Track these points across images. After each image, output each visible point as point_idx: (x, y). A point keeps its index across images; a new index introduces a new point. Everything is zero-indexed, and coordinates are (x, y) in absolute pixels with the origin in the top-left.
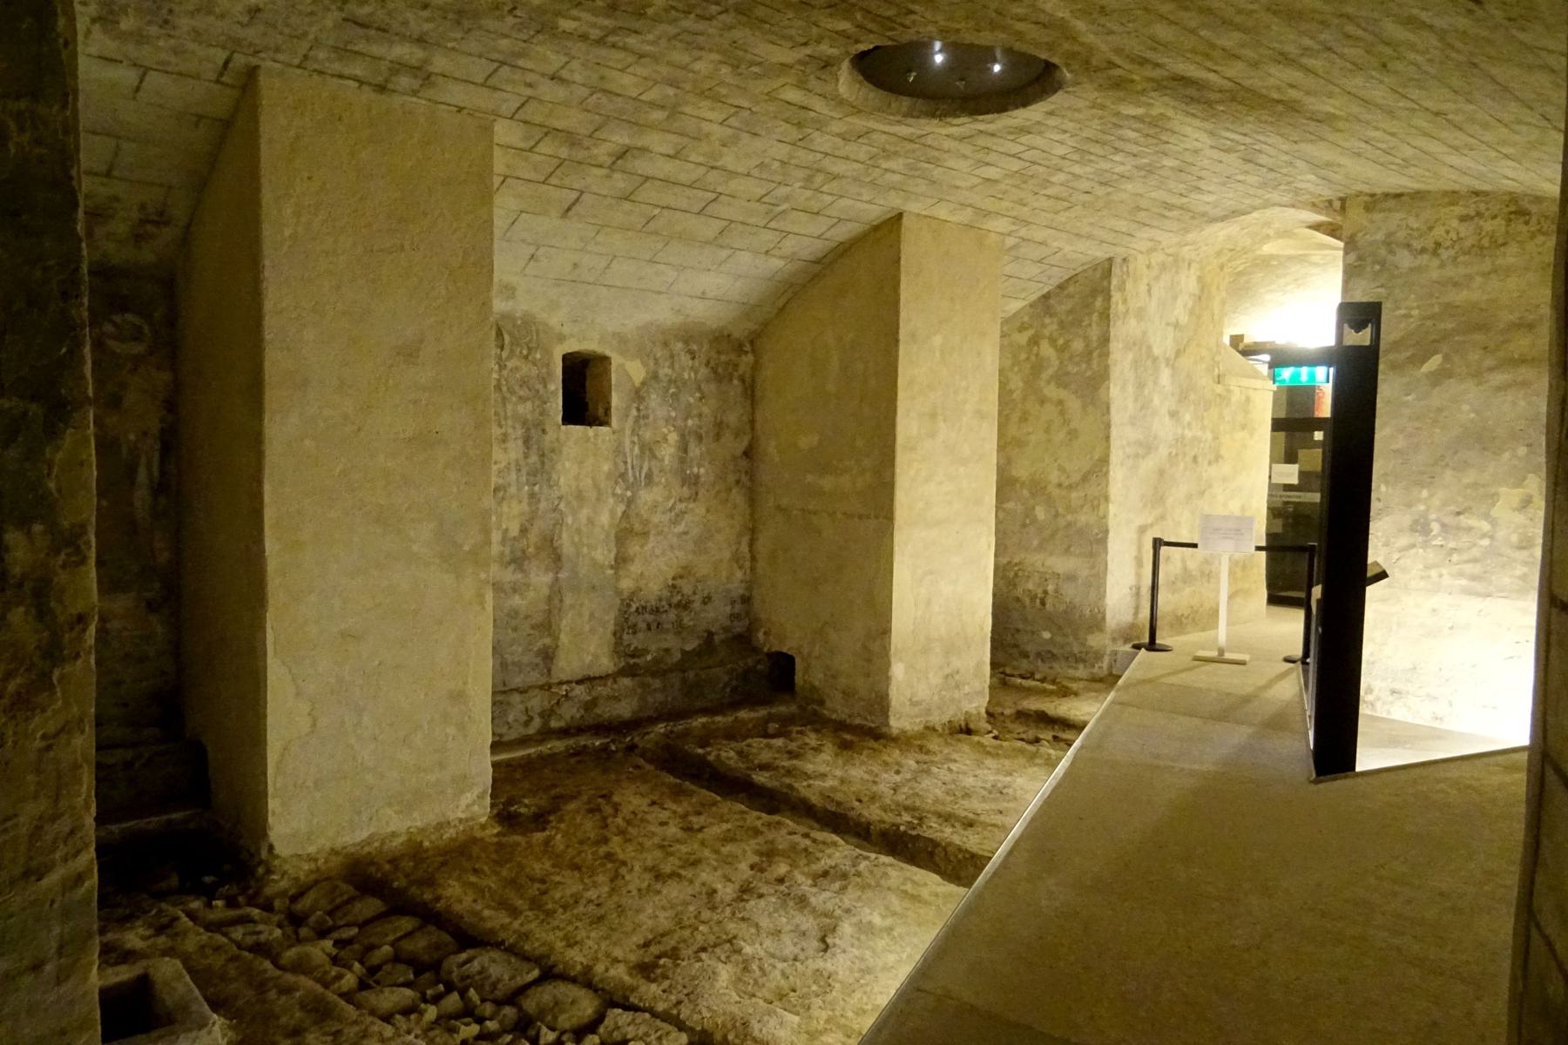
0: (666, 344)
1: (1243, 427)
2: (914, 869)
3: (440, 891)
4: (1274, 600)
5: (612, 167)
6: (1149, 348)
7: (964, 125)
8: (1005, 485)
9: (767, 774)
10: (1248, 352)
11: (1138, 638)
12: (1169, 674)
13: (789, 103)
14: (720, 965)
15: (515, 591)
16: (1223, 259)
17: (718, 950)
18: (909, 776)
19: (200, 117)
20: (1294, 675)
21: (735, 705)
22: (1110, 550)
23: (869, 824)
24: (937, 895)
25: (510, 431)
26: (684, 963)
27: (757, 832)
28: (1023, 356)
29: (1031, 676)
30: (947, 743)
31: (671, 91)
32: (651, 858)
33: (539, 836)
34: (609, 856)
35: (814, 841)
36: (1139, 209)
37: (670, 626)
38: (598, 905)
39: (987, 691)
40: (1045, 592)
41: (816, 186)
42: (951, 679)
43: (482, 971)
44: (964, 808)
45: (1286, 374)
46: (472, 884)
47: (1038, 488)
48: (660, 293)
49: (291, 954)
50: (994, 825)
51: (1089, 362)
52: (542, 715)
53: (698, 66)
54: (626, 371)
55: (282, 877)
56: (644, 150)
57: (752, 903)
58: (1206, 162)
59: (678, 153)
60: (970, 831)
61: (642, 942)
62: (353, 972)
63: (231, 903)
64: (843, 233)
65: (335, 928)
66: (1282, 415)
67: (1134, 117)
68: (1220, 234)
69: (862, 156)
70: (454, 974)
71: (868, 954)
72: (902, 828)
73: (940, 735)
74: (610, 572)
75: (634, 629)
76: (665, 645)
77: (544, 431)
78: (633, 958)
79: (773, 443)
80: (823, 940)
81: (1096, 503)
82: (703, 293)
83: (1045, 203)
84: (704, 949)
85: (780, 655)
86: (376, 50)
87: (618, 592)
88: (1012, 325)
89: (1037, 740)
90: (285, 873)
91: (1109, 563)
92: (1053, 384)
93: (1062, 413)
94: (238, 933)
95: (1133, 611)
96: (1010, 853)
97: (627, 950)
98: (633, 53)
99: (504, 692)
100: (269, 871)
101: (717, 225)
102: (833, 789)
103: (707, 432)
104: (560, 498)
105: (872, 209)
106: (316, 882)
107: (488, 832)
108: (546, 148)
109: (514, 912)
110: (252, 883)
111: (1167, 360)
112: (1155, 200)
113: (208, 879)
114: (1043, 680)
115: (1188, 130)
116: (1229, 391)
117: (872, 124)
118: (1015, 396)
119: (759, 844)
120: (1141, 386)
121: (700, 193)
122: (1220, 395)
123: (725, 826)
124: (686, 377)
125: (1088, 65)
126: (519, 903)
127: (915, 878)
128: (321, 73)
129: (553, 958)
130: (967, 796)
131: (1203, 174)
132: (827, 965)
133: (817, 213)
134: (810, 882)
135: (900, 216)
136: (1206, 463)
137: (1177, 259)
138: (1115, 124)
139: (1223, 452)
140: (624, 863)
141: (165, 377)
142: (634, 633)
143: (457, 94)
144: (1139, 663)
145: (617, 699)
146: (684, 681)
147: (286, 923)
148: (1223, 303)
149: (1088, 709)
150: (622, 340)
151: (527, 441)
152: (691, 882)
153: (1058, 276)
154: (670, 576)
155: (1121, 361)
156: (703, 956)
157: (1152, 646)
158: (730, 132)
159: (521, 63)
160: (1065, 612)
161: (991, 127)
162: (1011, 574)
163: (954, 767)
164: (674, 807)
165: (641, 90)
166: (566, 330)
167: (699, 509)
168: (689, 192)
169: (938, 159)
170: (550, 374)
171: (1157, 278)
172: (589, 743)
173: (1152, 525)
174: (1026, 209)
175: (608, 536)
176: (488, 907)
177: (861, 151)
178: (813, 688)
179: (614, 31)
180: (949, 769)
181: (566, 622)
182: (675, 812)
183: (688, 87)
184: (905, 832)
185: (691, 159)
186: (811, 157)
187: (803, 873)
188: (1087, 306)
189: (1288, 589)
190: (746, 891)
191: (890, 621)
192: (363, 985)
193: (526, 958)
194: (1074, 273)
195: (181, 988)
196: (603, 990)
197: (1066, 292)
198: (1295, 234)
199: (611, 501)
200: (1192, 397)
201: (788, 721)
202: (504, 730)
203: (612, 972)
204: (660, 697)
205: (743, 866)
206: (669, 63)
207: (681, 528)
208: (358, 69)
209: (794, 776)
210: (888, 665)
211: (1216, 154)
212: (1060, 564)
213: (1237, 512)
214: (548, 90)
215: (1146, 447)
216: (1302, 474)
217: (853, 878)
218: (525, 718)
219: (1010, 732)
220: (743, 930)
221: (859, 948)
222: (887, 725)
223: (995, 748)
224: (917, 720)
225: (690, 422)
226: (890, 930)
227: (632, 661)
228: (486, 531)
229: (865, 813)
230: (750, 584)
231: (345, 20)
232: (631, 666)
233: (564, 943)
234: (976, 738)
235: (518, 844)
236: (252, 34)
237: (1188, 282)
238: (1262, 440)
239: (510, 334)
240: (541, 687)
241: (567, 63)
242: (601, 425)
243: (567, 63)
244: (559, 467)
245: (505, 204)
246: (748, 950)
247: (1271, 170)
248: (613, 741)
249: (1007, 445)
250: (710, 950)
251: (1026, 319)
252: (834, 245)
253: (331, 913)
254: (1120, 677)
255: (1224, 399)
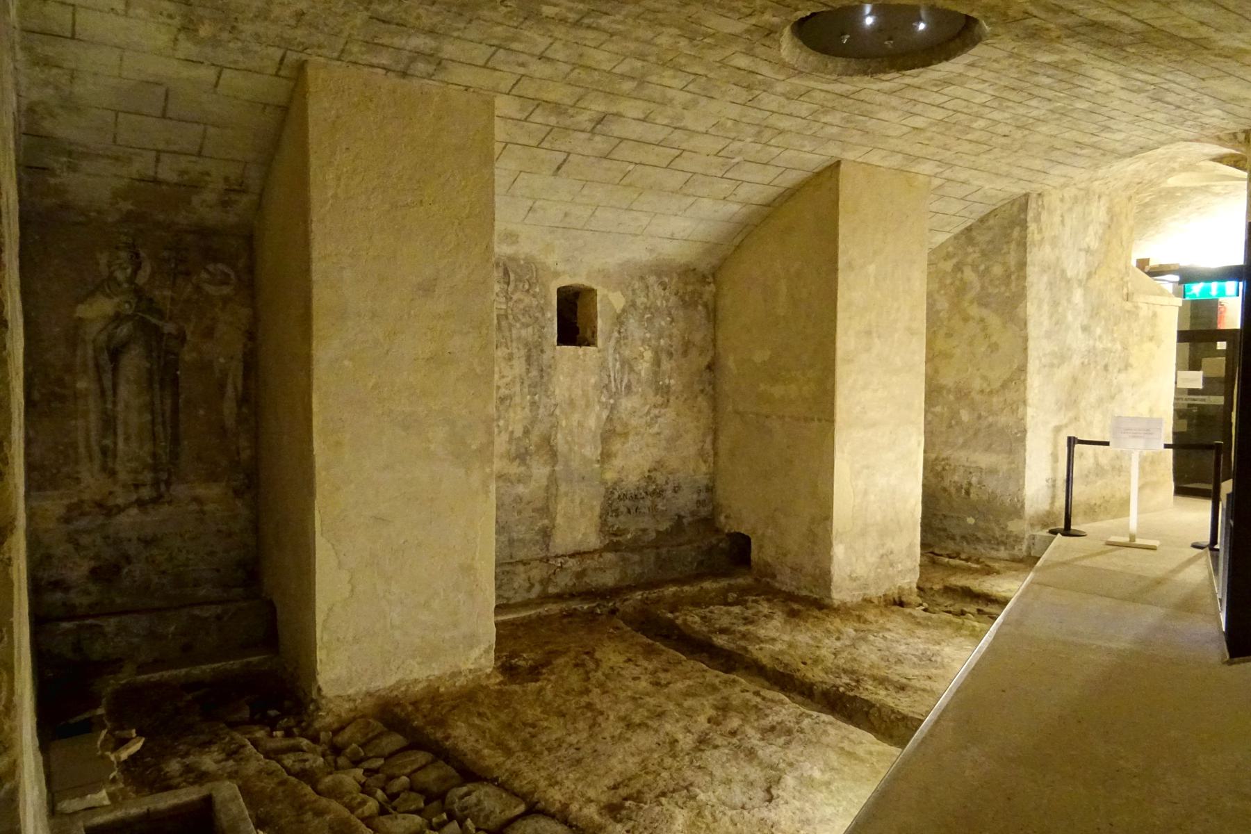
0: (642, 278)
1: (1151, 339)
2: (852, 728)
3: (449, 731)
4: (1182, 490)
5: (592, 131)
6: (1063, 271)
7: (892, 81)
8: (933, 392)
9: (725, 637)
10: (1155, 273)
11: (1055, 524)
12: (1084, 558)
13: (739, 69)
14: (677, 810)
15: (519, 481)
16: (1131, 192)
17: (676, 795)
18: (848, 643)
19: (266, 105)
20: (1203, 561)
21: (699, 577)
22: (1027, 447)
23: (812, 684)
24: (871, 753)
25: (515, 351)
26: (646, 807)
27: (714, 689)
28: (948, 281)
29: (957, 556)
30: (882, 614)
31: (639, 64)
32: (623, 709)
33: (532, 686)
34: (589, 706)
35: (764, 698)
36: (1053, 148)
37: (646, 511)
38: (578, 749)
39: (918, 569)
40: (970, 484)
41: (764, 140)
42: (887, 559)
43: (479, 802)
44: (896, 673)
45: (1196, 290)
46: (478, 727)
47: (962, 394)
48: (636, 235)
49: (328, 780)
50: (924, 690)
51: (1008, 285)
52: (541, 582)
53: (659, 41)
54: (609, 301)
55: (328, 714)
56: (618, 115)
57: (708, 753)
58: (1117, 102)
59: (647, 117)
60: (901, 694)
61: (612, 784)
62: (375, 798)
63: (288, 734)
64: (791, 179)
65: (367, 758)
66: (1187, 327)
67: (1049, 64)
68: (1128, 168)
69: (804, 113)
70: (455, 806)
71: (808, 806)
72: (841, 689)
73: (877, 607)
74: (597, 466)
75: (617, 513)
76: (642, 526)
77: (542, 351)
78: (604, 799)
79: (731, 358)
80: (768, 790)
81: (1014, 407)
82: (673, 234)
83: (967, 147)
84: (663, 794)
85: (743, 536)
86: (397, 42)
87: (603, 482)
88: (937, 255)
89: (963, 613)
90: (330, 710)
91: (1027, 458)
92: (975, 305)
93: (984, 329)
94: (289, 760)
95: (1049, 501)
96: (937, 723)
97: (599, 791)
98: (605, 31)
99: (511, 563)
100: (318, 709)
101: (681, 177)
102: (782, 652)
103: (676, 350)
104: (556, 405)
105: (813, 158)
106: (354, 719)
107: (493, 681)
108: (538, 117)
109: (509, 752)
110: (306, 718)
111: (1080, 281)
112: (1068, 140)
113: (273, 713)
114: (967, 560)
115: (1099, 74)
116: (1137, 307)
117: (812, 84)
118: (941, 314)
119: (715, 700)
120: (1055, 304)
121: (668, 150)
122: (1128, 312)
123: (688, 682)
124: (659, 303)
125: (1005, 19)
126: (513, 744)
127: (852, 736)
128: (355, 63)
129: (536, 796)
130: (899, 661)
131: (1113, 114)
132: (771, 815)
133: (766, 164)
134: (759, 736)
135: (838, 163)
136: (1116, 370)
137: (1087, 191)
138: (1030, 72)
139: (1132, 360)
140: (602, 713)
141: (245, 312)
142: (617, 516)
143: (464, 76)
144: (1055, 548)
145: (603, 570)
146: (658, 556)
147: (328, 752)
148: (1132, 230)
149: (1009, 586)
150: (605, 275)
151: (528, 359)
152: (656, 731)
153: (980, 210)
154: (646, 469)
155: (1037, 284)
156: (663, 800)
157: (1067, 531)
158: (689, 96)
159: (515, 46)
160: (989, 501)
161: (917, 81)
162: (939, 468)
163: (888, 635)
164: (646, 664)
165: (613, 65)
166: (560, 268)
167: (670, 413)
168: (657, 148)
169: (872, 112)
170: (548, 303)
171: (1070, 209)
172: (578, 607)
173: (1066, 426)
174: (949, 153)
175: (594, 437)
176: (487, 747)
177: (803, 108)
178: (767, 564)
179: (588, 14)
180: (884, 638)
181: (561, 507)
182: (646, 669)
183: (652, 59)
184: (844, 693)
185: (658, 121)
186: (760, 115)
187: (753, 727)
188: (1006, 237)
189: (1189, 483)
190: (703, 742)
191: (831, 508)
192: (383, 811)
193: (515, 794)
194: (994, 207)
195: (235, 810)
196: (577, 826)
197: (986, 224)
198: (1199, 167)
199: (597, 408)
200: (1103, 313)
201: (744, 591)
202: (510, 594)
203: (585, 811)
204: (638, 570)
205: (702, 719)
206: (637, 39)
207: (655, 429)
208: (384, 60)
209: (748, 640)
210: (831, 545)
211: (1125, 95)
212: (983, 459)
213: (1146, 414)
214: (539, 69)
215: (1062, 358)
216: (1206, 380)
217: (796, 734)
218: (528, 585)
219: (938, 605)
220: (701, 779)
221: (799, 800)
222: (830, 597)
223: (925, 619)
224: (856, 593)
225: (662, 342)
226: (828, 784)
227: (615, 539)
228: (490, 433)
229: (809, 675)
230: (713, 476)
231: (371, 18)
232: (614, 543)
233: (547, 782)
234: (908, 610)
235: (516, 692)
236: (300, 34)
237: (1099, 212)
238: (1168, 349)
239: (515, 273)
240: (541, 560)
241: (552, 44)
242: (588, 345)
243: (552, 44)
244: (554, 379)
245: (504, 170)
246: (702, 797)
247: (1179, 107)
248: (598, 606)
249: (932, 357)
250: (669, 795)
251: (951, 249)
252: (781, 190)
253: (363, 746)
254: (1039, 558)
255: (1133, 314)
